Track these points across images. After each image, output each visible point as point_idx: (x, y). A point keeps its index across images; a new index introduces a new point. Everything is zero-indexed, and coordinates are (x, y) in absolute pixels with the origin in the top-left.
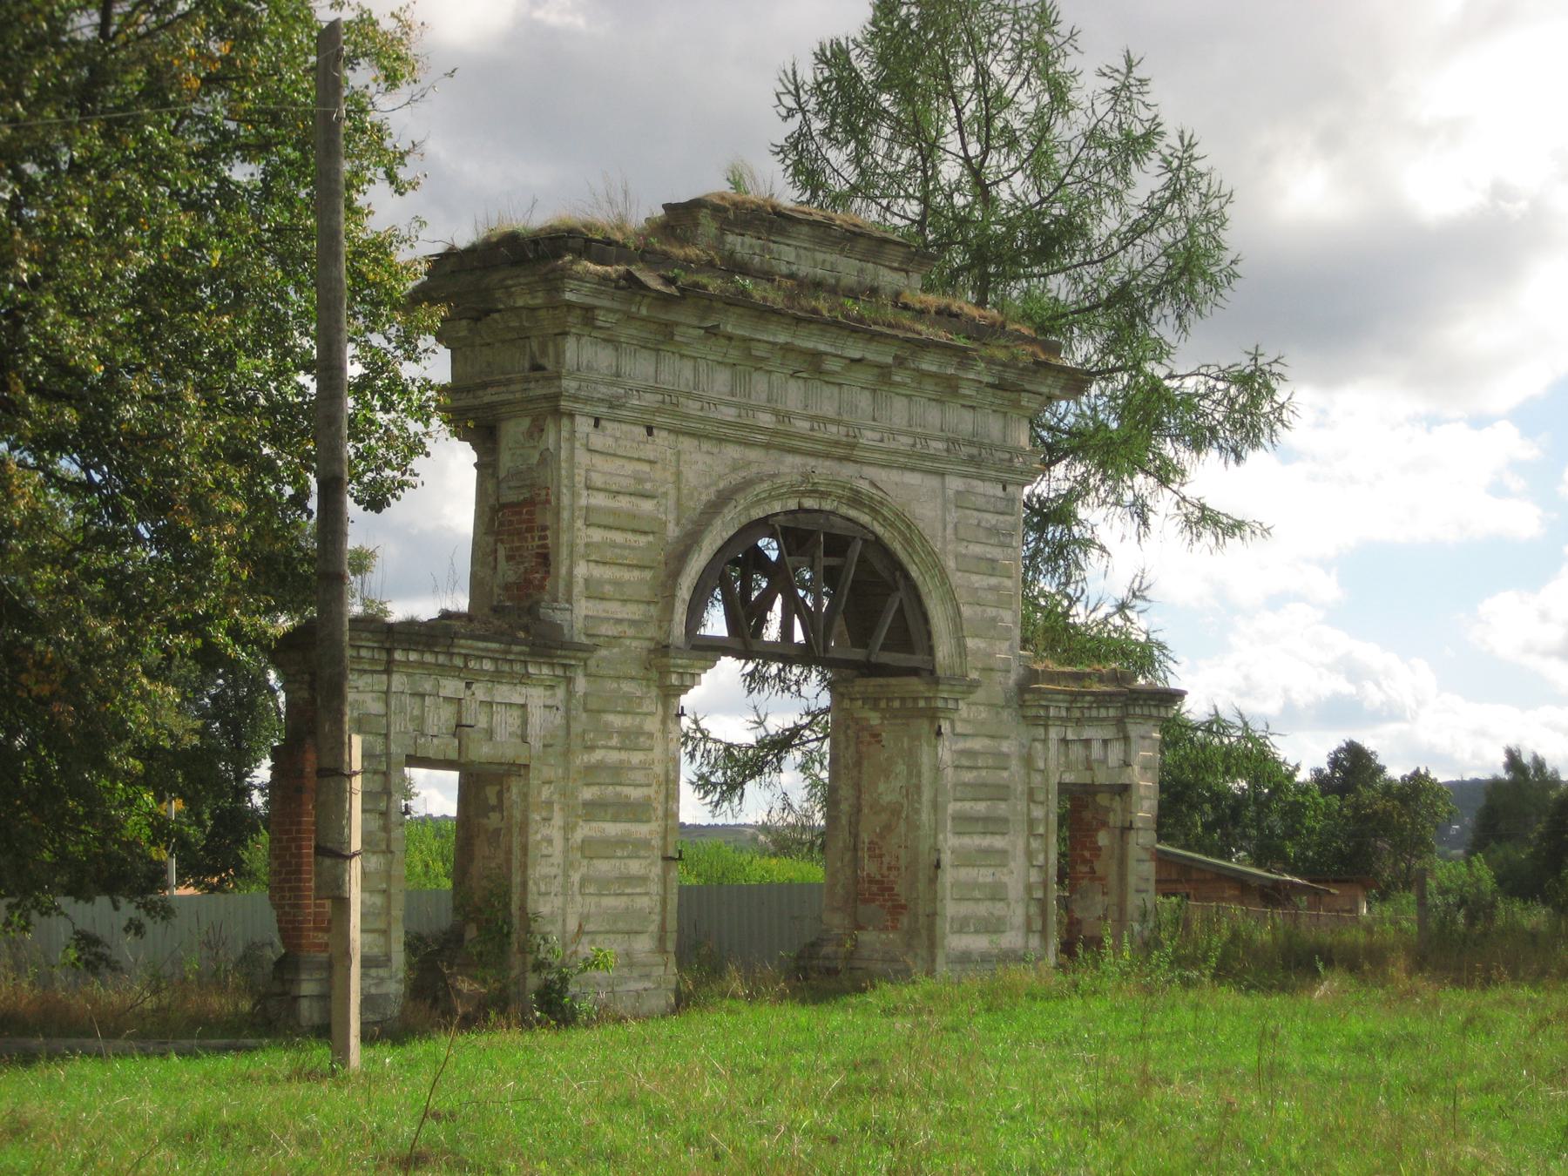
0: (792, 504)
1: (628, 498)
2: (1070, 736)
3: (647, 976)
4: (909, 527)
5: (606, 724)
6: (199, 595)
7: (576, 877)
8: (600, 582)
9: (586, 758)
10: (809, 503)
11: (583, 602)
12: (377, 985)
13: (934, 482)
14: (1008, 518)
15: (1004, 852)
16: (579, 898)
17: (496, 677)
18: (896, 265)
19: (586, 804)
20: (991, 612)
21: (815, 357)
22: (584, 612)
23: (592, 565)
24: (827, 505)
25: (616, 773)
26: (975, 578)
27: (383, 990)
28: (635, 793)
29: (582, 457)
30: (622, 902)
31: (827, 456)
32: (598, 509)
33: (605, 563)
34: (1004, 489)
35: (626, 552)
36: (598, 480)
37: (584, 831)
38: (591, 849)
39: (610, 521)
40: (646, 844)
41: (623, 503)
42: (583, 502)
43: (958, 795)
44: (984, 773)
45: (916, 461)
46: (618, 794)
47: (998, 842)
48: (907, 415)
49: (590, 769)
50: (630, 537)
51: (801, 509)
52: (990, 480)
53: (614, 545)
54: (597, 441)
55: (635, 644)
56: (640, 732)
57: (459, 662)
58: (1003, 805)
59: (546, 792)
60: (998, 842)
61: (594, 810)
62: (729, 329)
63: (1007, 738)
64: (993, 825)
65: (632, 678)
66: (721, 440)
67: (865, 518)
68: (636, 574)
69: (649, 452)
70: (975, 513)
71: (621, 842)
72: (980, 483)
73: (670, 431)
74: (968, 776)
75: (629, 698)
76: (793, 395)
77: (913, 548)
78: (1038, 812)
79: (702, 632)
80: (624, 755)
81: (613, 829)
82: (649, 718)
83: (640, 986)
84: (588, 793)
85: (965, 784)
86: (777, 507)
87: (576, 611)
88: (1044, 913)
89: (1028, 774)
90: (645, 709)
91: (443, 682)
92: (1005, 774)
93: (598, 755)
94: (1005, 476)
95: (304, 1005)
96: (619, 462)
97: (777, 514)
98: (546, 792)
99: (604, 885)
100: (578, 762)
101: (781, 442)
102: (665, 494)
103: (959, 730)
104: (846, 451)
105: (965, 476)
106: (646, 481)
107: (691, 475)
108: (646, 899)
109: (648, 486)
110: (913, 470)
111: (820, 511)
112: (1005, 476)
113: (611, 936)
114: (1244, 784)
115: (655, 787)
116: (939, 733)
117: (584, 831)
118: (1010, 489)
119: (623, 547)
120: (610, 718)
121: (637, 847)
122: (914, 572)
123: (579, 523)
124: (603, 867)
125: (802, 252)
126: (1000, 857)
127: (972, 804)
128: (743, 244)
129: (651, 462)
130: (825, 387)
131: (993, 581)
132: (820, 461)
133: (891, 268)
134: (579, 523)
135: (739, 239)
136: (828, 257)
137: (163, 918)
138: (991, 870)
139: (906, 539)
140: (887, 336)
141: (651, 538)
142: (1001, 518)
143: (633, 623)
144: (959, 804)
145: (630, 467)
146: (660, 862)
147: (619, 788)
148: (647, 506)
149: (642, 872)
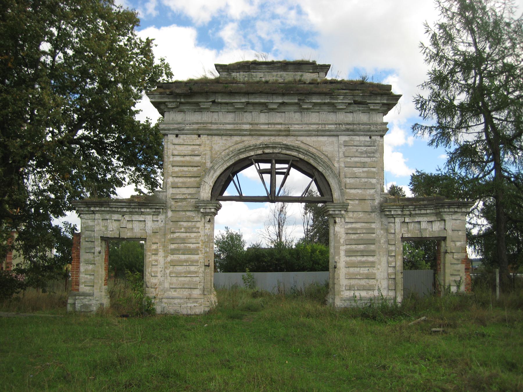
1: (189, 157)
3: (196, 302)
4: (313, 154)
5: (180, 225)
7: (168, 272)
8: (177, 183)
9: (172, 236)
10: (267, 151)
11: (171, 189)
12: (88, 301)
13: (334, 139)
14: (373, 147)
16: (169, 278)
17: (131, 213)
18: (311, 71)
19: (172, 250)
21: (265, 105)
22: (171, 192)
23: (174, 178)
24: (276, 151)
25: (184, 241)
27: (91, 303)
30: (187, 279)
31: (279, 135)
33: (180, 177)
34: (370, 138)
35: (187, 173)
37: (170, 258)
38: (173, 263)
39: (181, 164)
40: (197, 261)
41: (188, 158)
43: (347, 243)
44: (362, 235)
46: (186, 246)
49: (173, 239)
50: (190, 168)
51: (264, 153)
52: (362, 135)
53: (183, 171)
54: (176, 141)
55: (192, 200)
56: (195, 227)
58: (373, 246)
59: (154, 247)
61: (173, 252)
62: (219, 100)
63: (374, 222)
65: (191, 211)
66: (231, 135)
67: (295, 154)
68: (193, 179)
69: (198, 142)
71: (186, 261)
75: (189, 217)
77: (317, 161)
78: (392, 248)
80: (188, 234)
81: (183, 257)
82: (198, 223)
83: (193, 305)
84: (173, 246)
86: (252, 153)
87: (168, 192)
88: (396, 284)
89: (387, 235)
90: (195, 220)
91: (113, 215)
92: (374, 235)
93: (176, 235)
94: (369, 133)
95: (69, 306)
96: (185, 146)
97: (252, 156)
98: (154, 247)
99: (178, 275)
100: (169, 237)
101: (252, 133)
102: (205, 154)
103: (347, 221)
104: (288, 133)
105: (349, 135)
106: (195, 151)
107: (216, 148)
108: (198, 279)
109: (196, 152)
110: (323, 136)
111: (273, 153)
112: (369, 133)
113: (184, 290)
115: (201, 243)
116: (335, 222)
117: (170, 258)
118: (373, 138)
119: (186, 171)
120: (182, 223)
122: (320, 169)
124: (179, 268)
125: (266, 73)
127: (356, 246)
128: (240, 75)
129: (199, 145)
130: (278, 114)
132: (277, 137)
133: (310, 72)
135: (238, 74)
136: (279, 73)
137: (356, 297)
138: (367, 269)
139: (314, 159)
141: (199, 168)
143: (189, 194)
145: (190, 148)
146: (203, 267)
147: (185, 244)
148: (197, 158)
149: (196, 270)
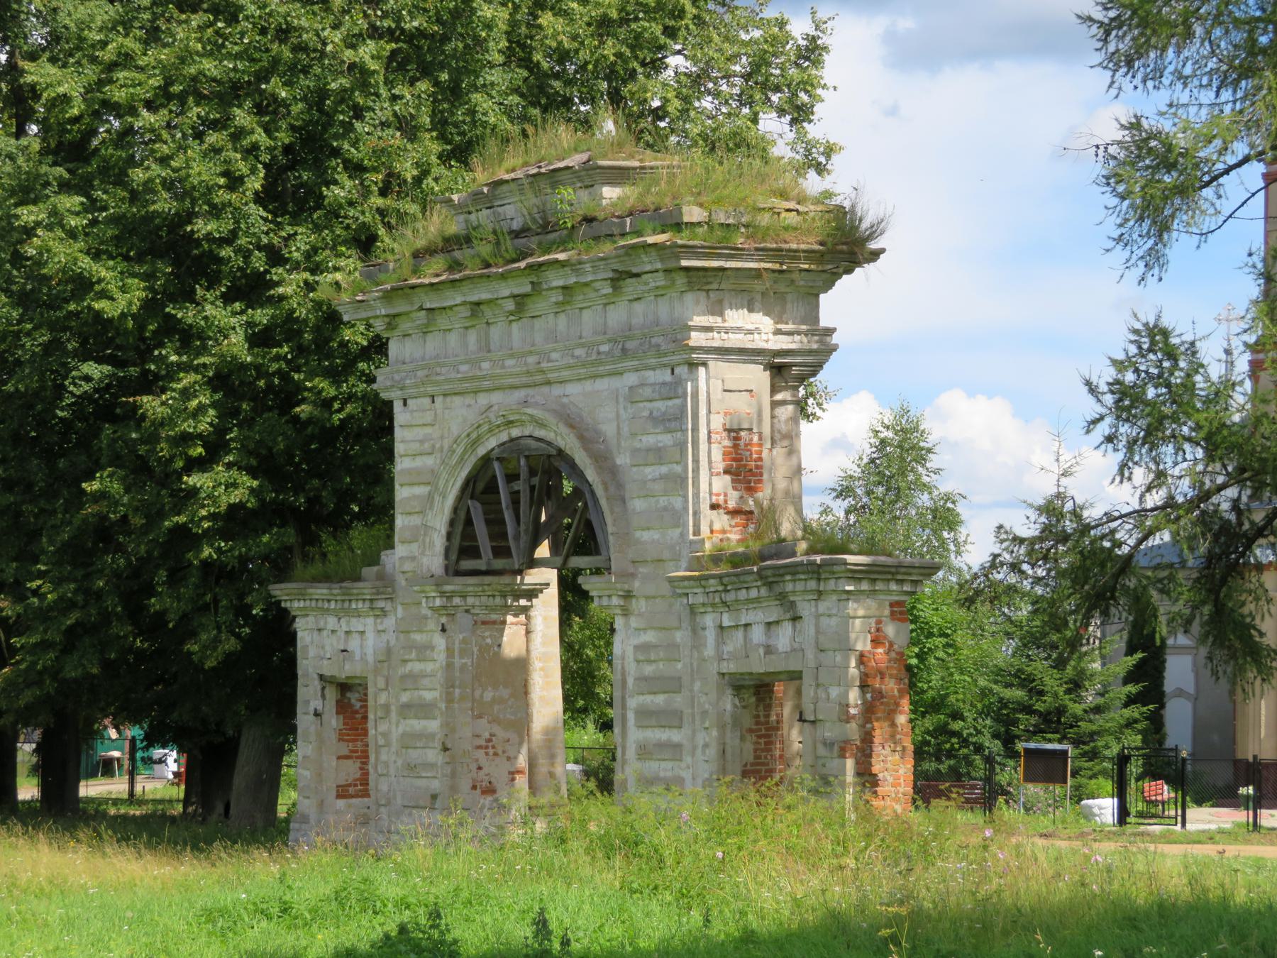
0: (504, 437)
2: (726, 623)
15: (677, 747)
20: (663, 501)
26: (648, 470)
40: (431, 736)
45: (593, 368)
47: (675, 736)
48: (550, 330)
57: (314, 603)
60: (675, 736)
64: (671, 718)
70: (648, 405)
72: (651, 373)
74: (648, 670)
79: (975, 549)
85: (646, 679)
93: (409, 666)
94: (430, 389)
97: (493, 449)
131: (664, 469)
140: (460, 280)
142: (670, 403)
144: (641, 698)
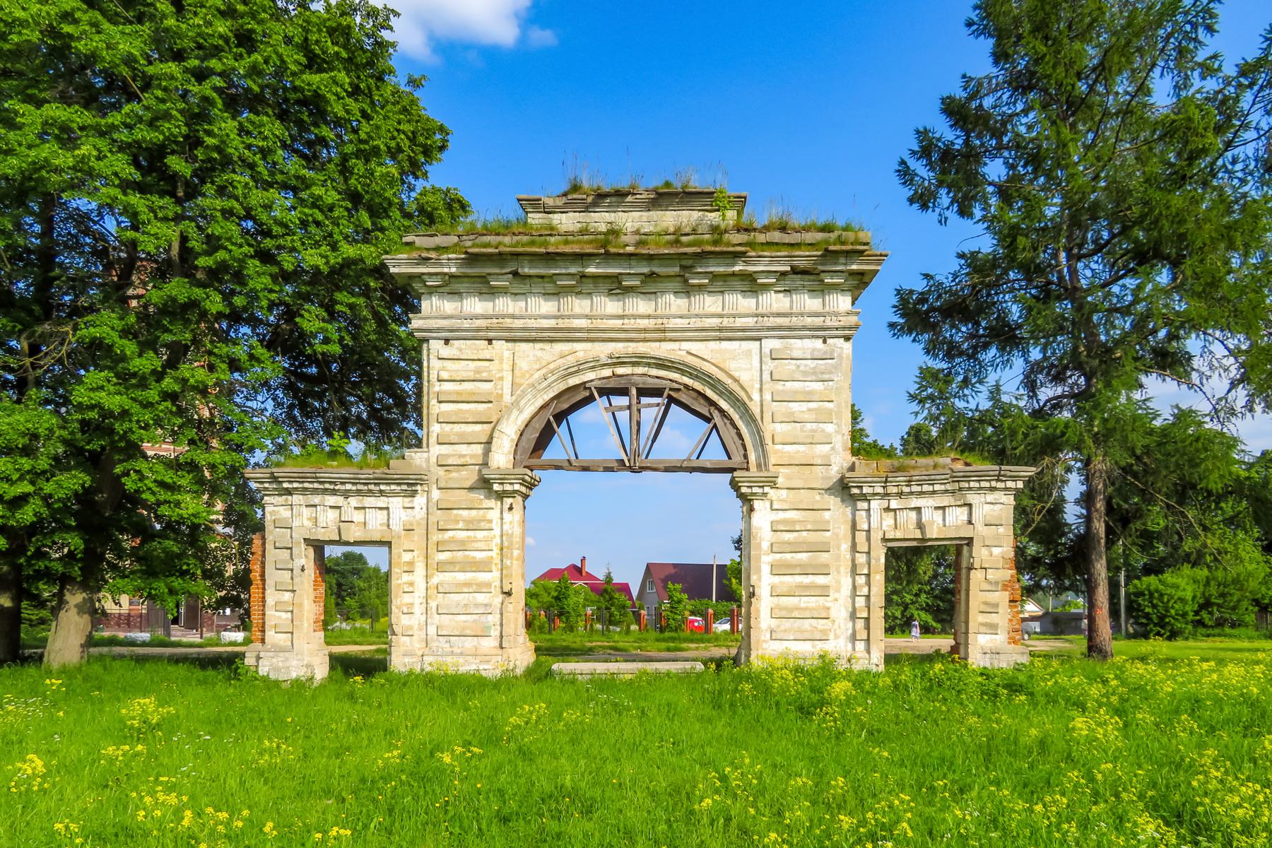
0: (607, 372)
6: (951, 342)
15: (826, 587)
21: (616, 278)
25: (463, 546)
28: (479, 556)
29: (435, 363)
32: (445, 393)
36: (444, 375)
40: (489, 585)
42: (437, 389)
46: (467, 556)
59: (407, 557)
61: (441, 567)
62: (526, 270)
73: (507, 341)
76: (610, 306)
81: (461, 577)
102: (501, 379)
107: (523, 364)
114: (270, 825)
117: (437, 578)
121: (482, 588)
123: (434, 402)
126: (824, 592)
134: (434, 402)
